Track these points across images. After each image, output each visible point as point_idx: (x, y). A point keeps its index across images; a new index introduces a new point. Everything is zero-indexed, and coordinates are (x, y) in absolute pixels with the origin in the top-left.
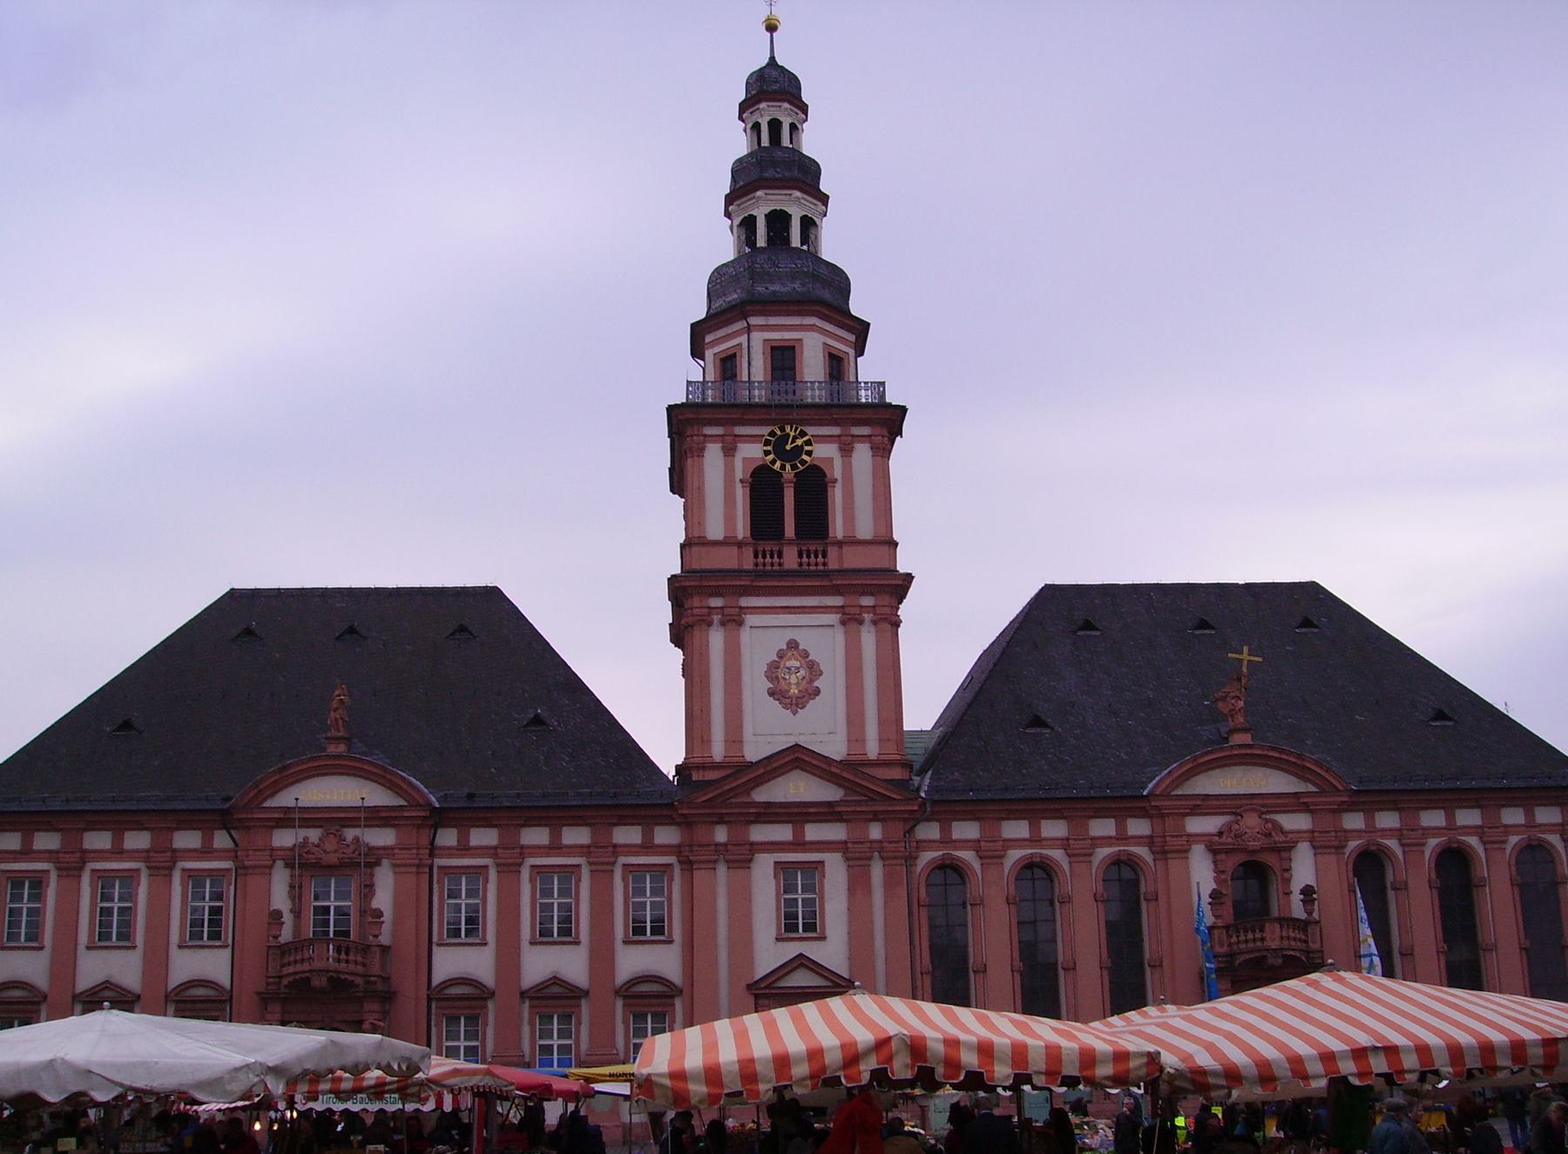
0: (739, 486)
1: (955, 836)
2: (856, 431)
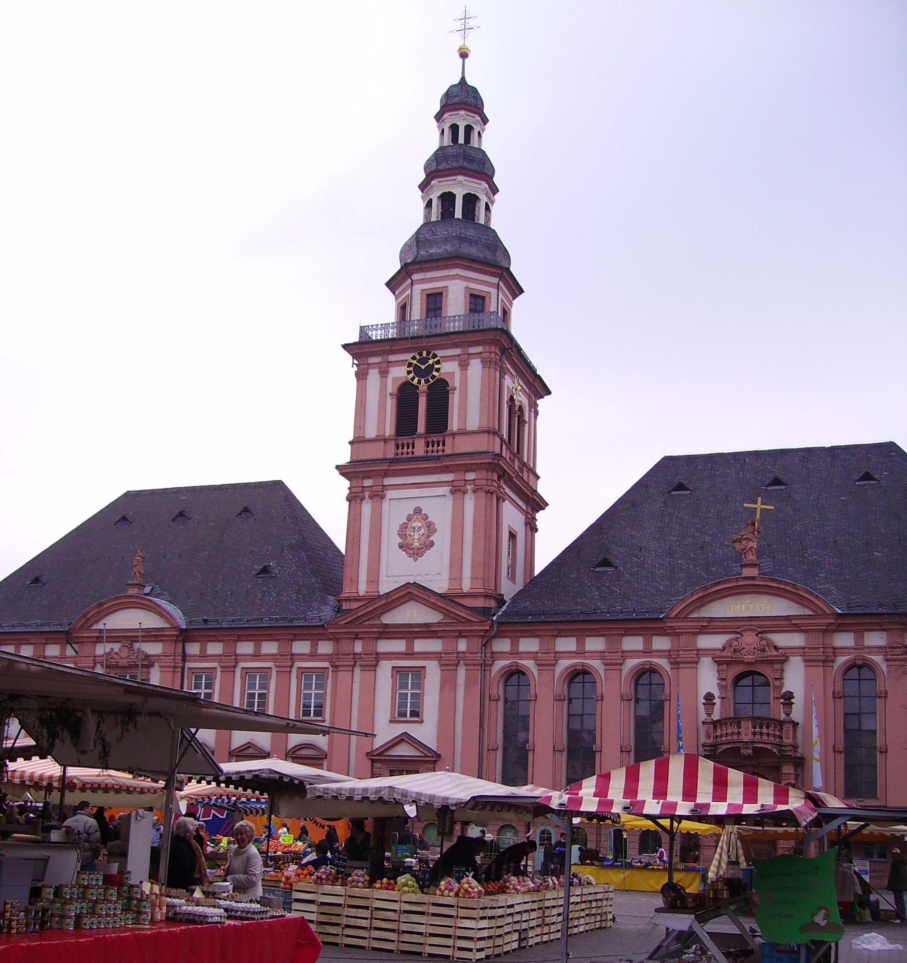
0: (389, 398)
1: (866, 644)
2: (472, 350)
